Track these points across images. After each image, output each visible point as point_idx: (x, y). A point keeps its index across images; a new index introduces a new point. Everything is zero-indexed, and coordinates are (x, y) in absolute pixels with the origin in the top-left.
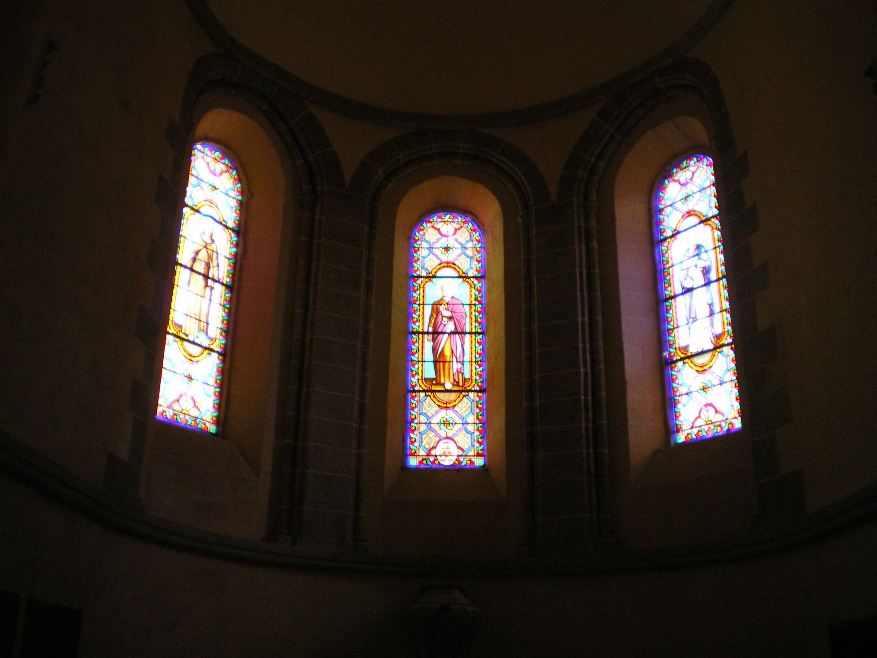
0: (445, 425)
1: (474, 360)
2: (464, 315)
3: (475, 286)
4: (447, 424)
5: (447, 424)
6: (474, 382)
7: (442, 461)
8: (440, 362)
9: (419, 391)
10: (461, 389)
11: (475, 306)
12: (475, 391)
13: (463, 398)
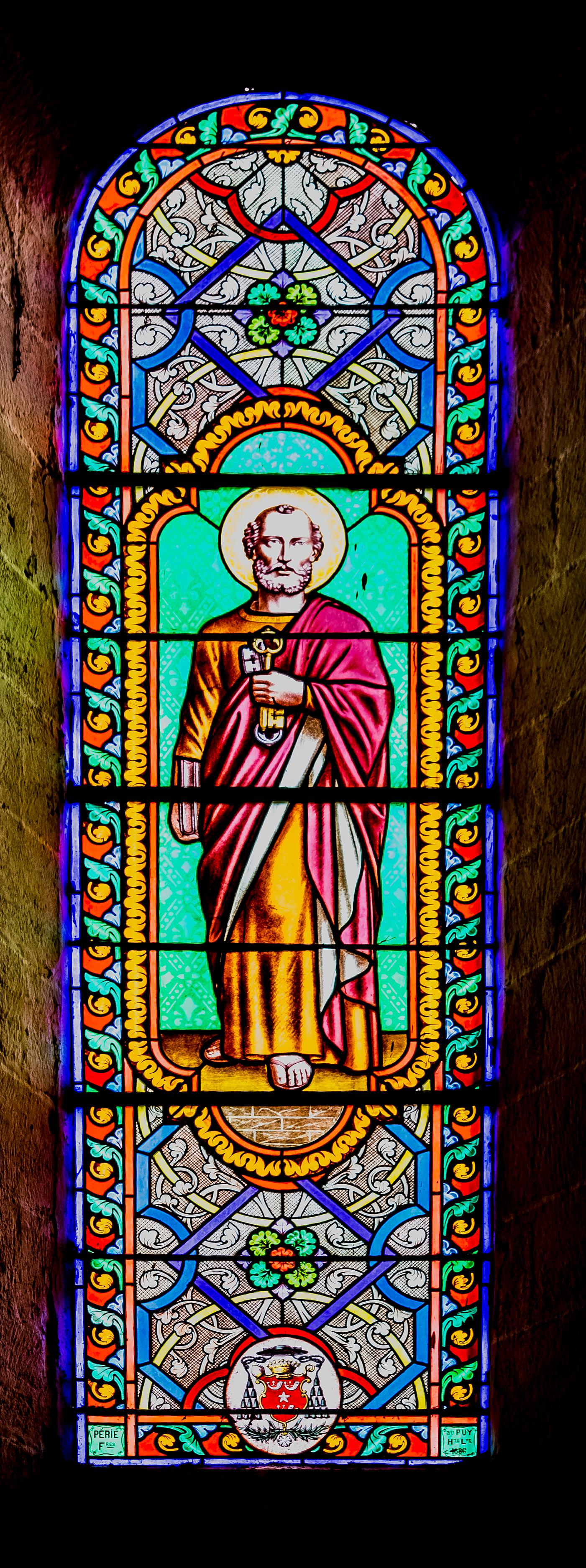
0: (276, 1265)
1: (431, 937)
2: (379, 695)
3: (444, 532)
4: (283, 1259)
5: (283, 1259)
6: (432, 1051)
7: (259, 1435)
8: (243, 947)
9: (133, 1100)
10: (361, 1085)
11: (444, 650)
13: (370, 1130)
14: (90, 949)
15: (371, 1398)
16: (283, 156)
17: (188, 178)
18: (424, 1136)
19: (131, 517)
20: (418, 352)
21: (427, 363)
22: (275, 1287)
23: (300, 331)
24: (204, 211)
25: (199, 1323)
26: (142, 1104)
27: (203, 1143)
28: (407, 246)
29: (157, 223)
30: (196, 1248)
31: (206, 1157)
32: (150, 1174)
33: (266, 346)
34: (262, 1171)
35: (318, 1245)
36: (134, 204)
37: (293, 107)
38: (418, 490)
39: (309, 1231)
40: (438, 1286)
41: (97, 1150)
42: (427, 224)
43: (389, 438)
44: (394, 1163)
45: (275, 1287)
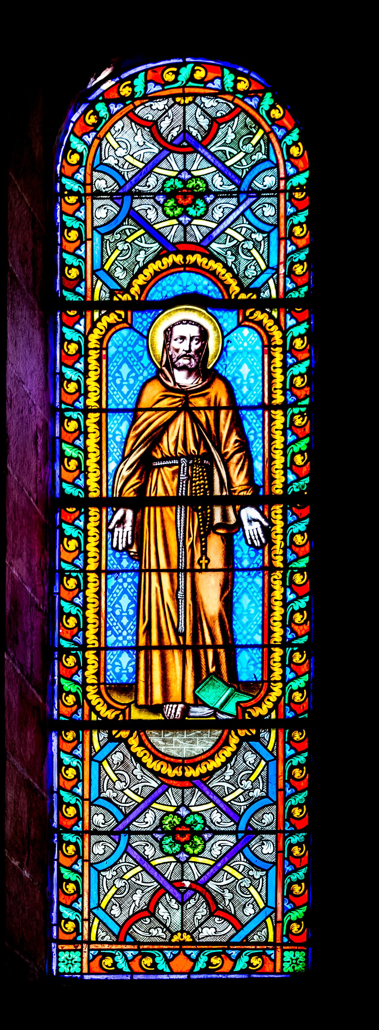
9: (90, 726)
15: (238, 932)
16: (182, 937)
17: (126, 115)
18: (97, 281)
19: (91, 332)
21: (272, 227)
22: (178, 853)
26: (95, 729)
27: (134, 755)
28: (261, 151)
31: (135, 764)
33: (194, 813)
36: (94, 130)
37: (190, 66)
38: (268, 310)
41: (67, 759)
43: (117, 753)
44: (254, 768)
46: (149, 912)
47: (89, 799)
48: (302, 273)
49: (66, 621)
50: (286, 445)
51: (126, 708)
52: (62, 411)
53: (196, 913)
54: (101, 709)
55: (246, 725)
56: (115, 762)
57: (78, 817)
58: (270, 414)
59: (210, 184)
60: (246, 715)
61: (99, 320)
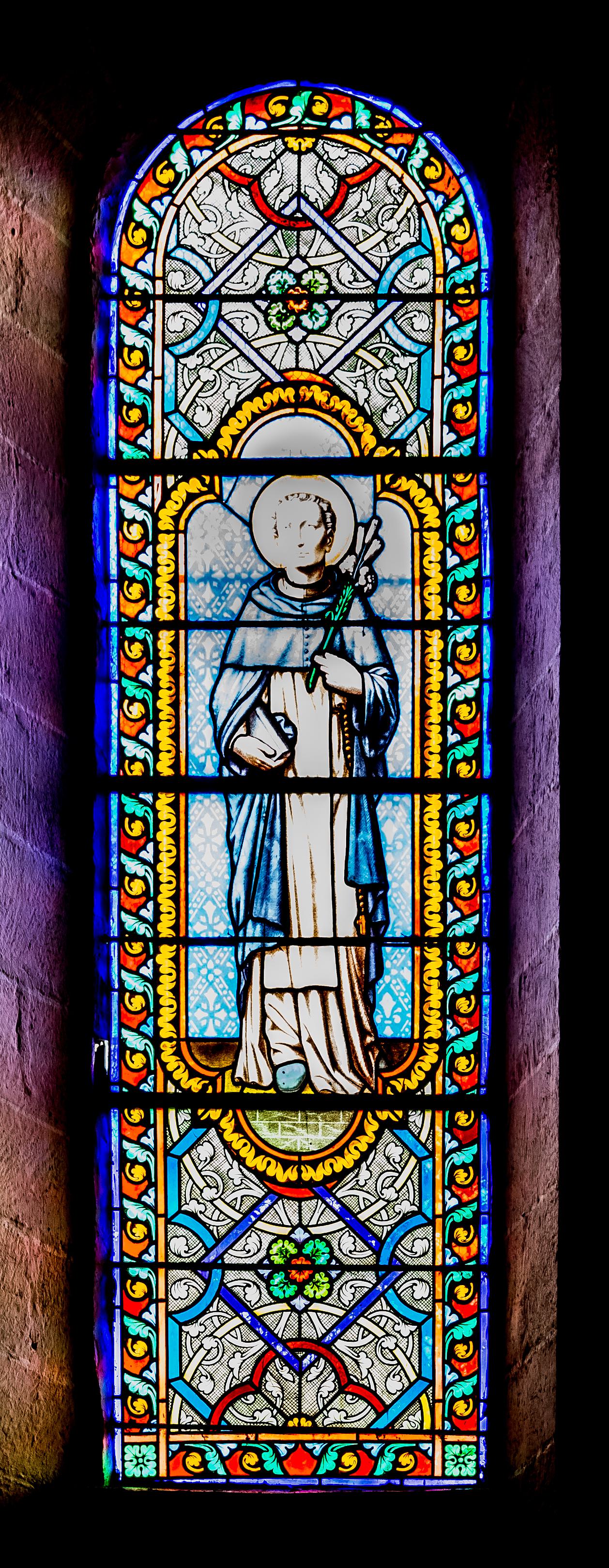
9: (164, 1101)
11: (444, 638)
12: (436, 1103)
13: (379, 1134)
14: (126, 944)
15: (379, 1416)
19: (162, 506)
20: (181, 1231)
23: (316, 285)
24: (369, 1372)
25: (376, 232)
29: (189, 212)
30: (221, 1257)
32: (418, 390)
34: (282, 1178)
35: (266, 314)
36: (169, 193)
38: (418, 475)
39: (322, 1239)
40: (441, 1297)
42: (426, 208)
43: (392, 424)
45: (305, 271)
46: (253, 1386)
47: (165, 1215)
48: (469, 895)
49: (128, 589)
50: (445, 748)
51: (217, 1077)
52: (124, 1267)
53: (320, 1388)
54: (181, 1075)
55: (390, 1103)
56: (202, 1158)
57: (150, 1239)
58: (423, 635)
59: (336, 1248)
60: (389, 1089)
61: (175, 487)
